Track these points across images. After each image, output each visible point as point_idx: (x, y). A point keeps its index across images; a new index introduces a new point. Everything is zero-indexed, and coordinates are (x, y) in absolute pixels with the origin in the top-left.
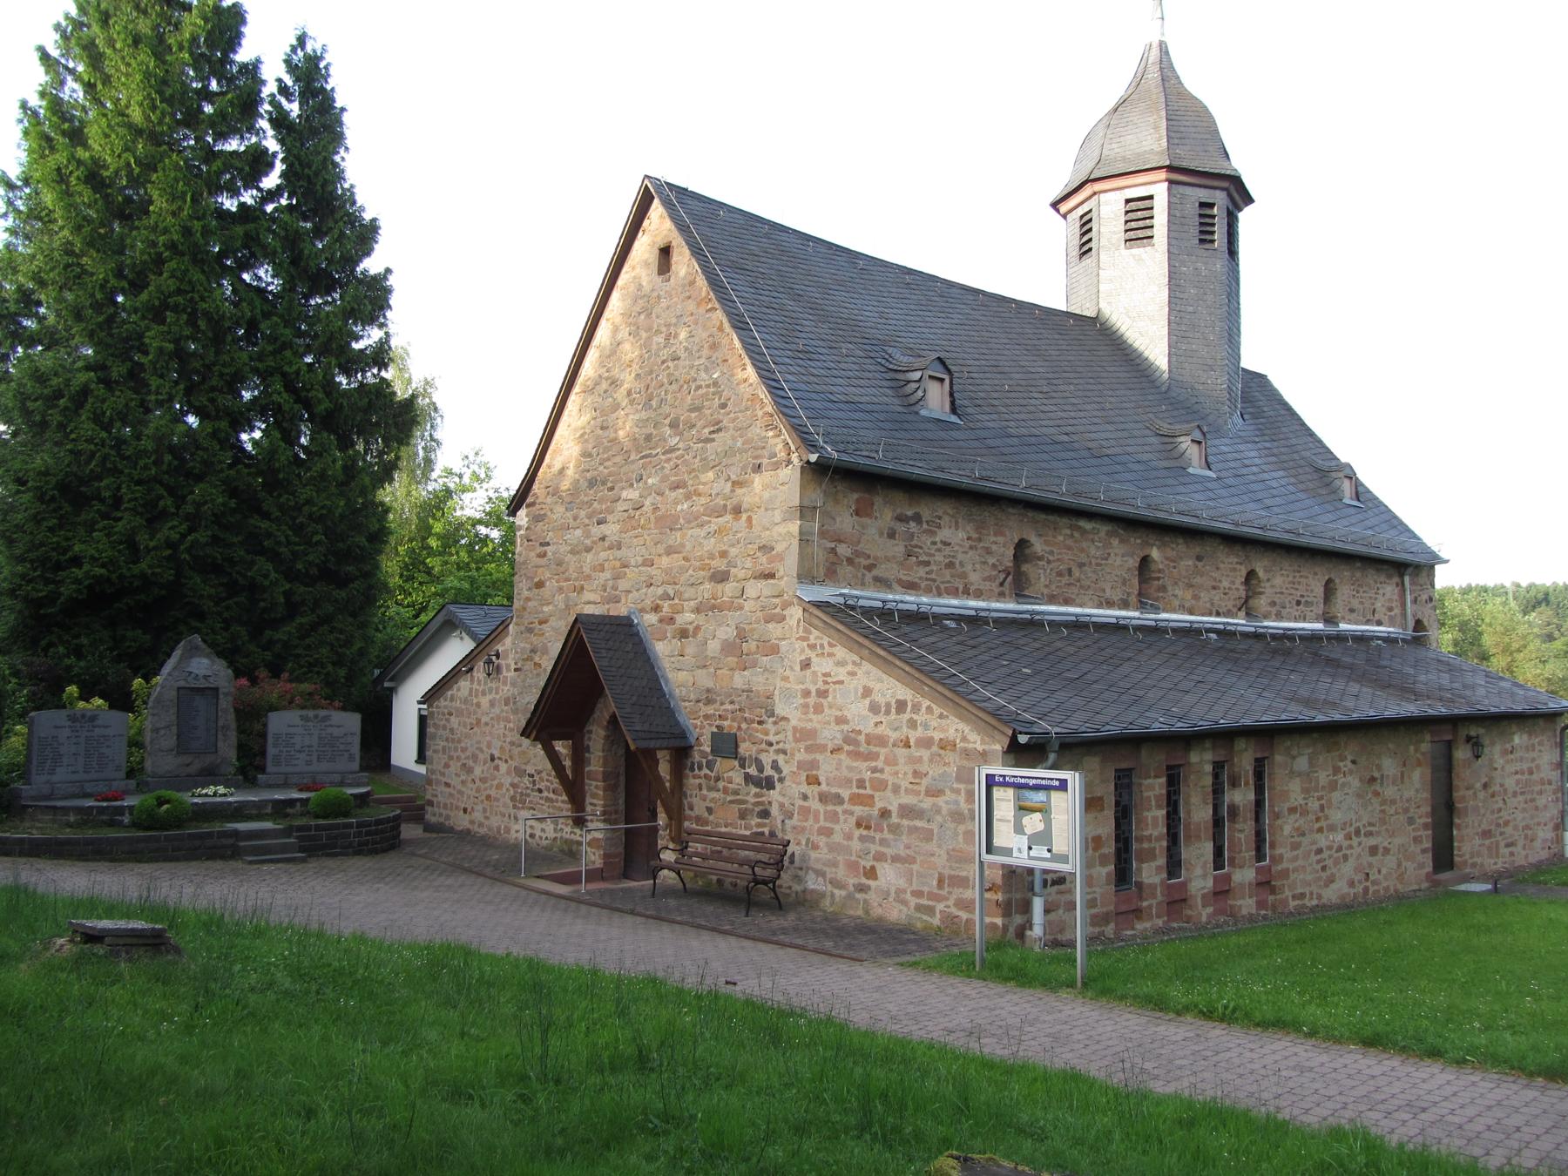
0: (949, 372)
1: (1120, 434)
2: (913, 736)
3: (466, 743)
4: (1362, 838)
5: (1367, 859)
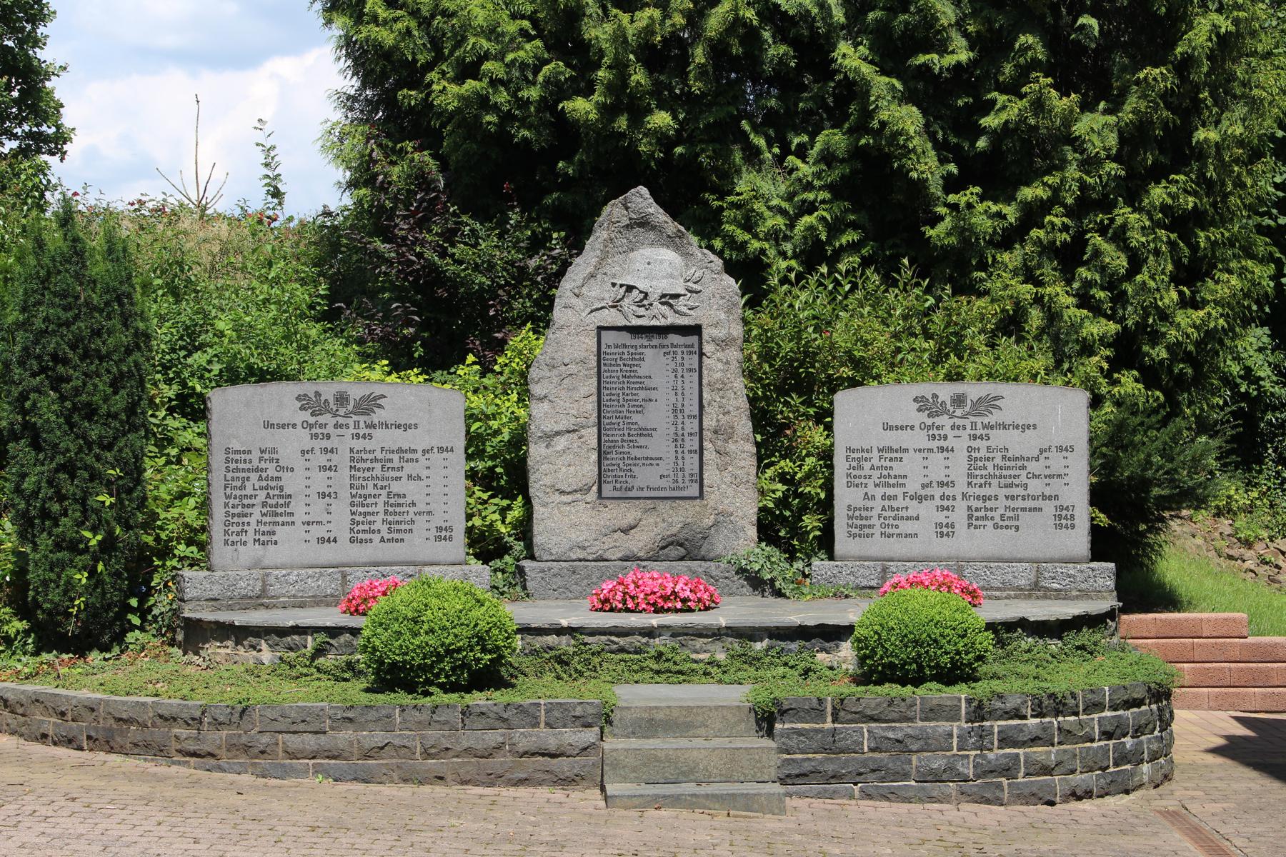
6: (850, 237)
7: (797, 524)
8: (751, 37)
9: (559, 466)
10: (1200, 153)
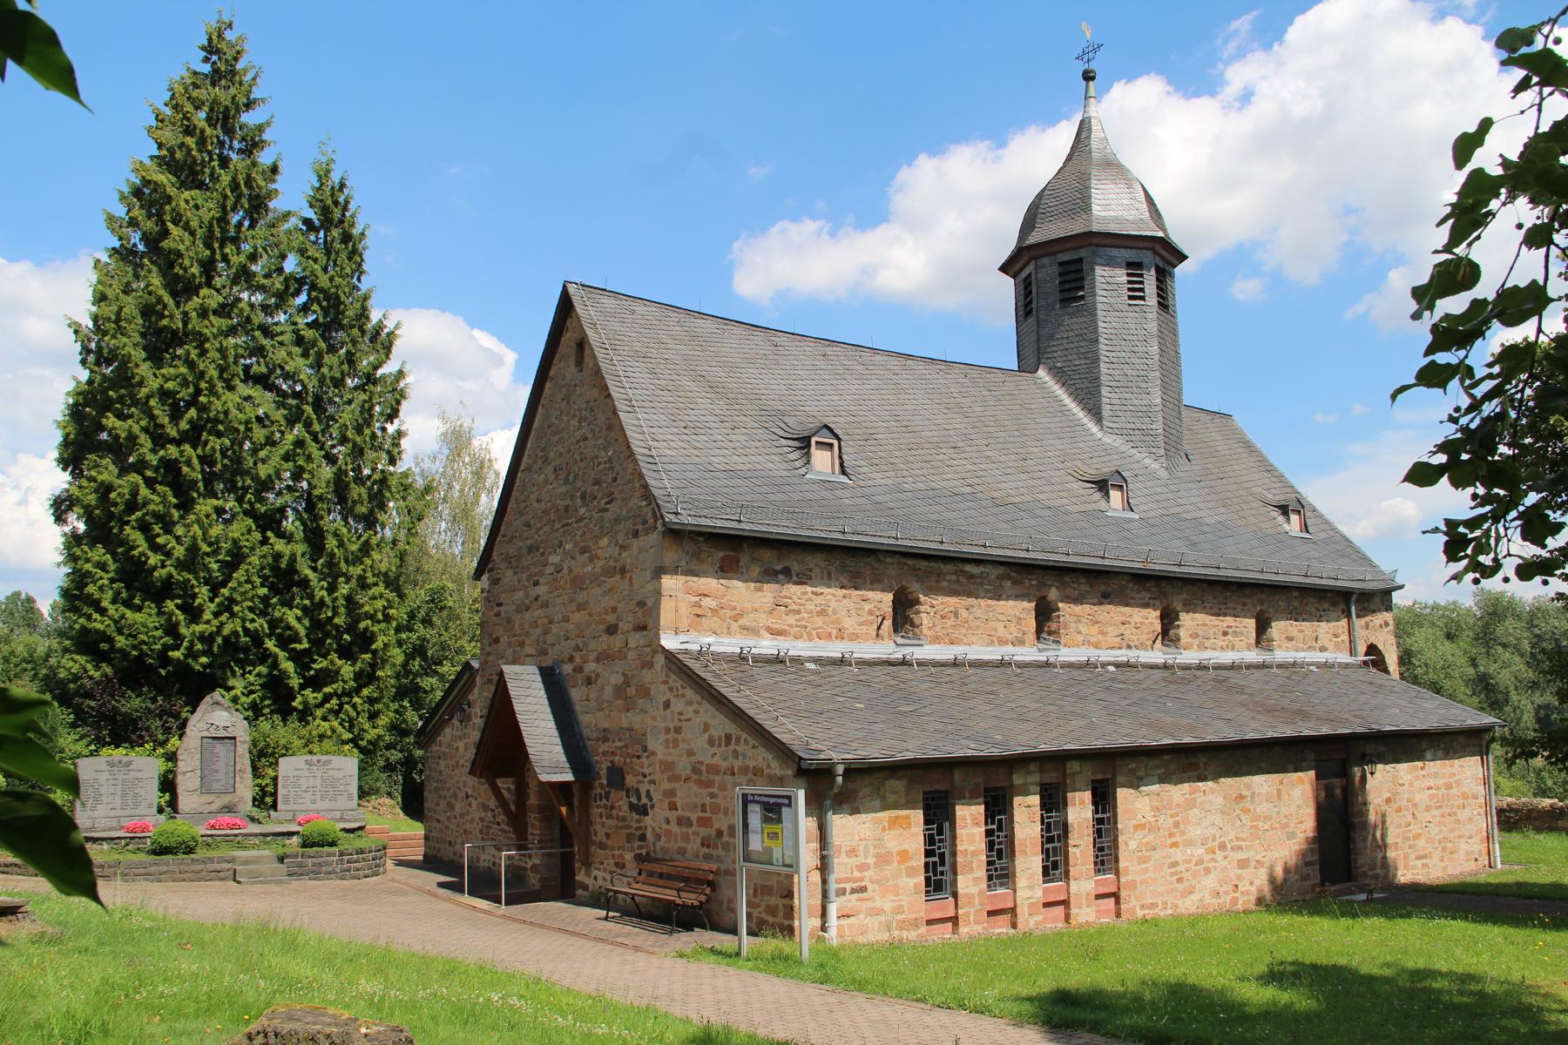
0: (839, 440)
1: (1034, 482)
2: (737, 764)
3: (450, 783)
4: (1229, 852)
5: (1234, 872)
6: (267, 702)
7: (266, 799)
9: (187, 783)
10: (378, 678)
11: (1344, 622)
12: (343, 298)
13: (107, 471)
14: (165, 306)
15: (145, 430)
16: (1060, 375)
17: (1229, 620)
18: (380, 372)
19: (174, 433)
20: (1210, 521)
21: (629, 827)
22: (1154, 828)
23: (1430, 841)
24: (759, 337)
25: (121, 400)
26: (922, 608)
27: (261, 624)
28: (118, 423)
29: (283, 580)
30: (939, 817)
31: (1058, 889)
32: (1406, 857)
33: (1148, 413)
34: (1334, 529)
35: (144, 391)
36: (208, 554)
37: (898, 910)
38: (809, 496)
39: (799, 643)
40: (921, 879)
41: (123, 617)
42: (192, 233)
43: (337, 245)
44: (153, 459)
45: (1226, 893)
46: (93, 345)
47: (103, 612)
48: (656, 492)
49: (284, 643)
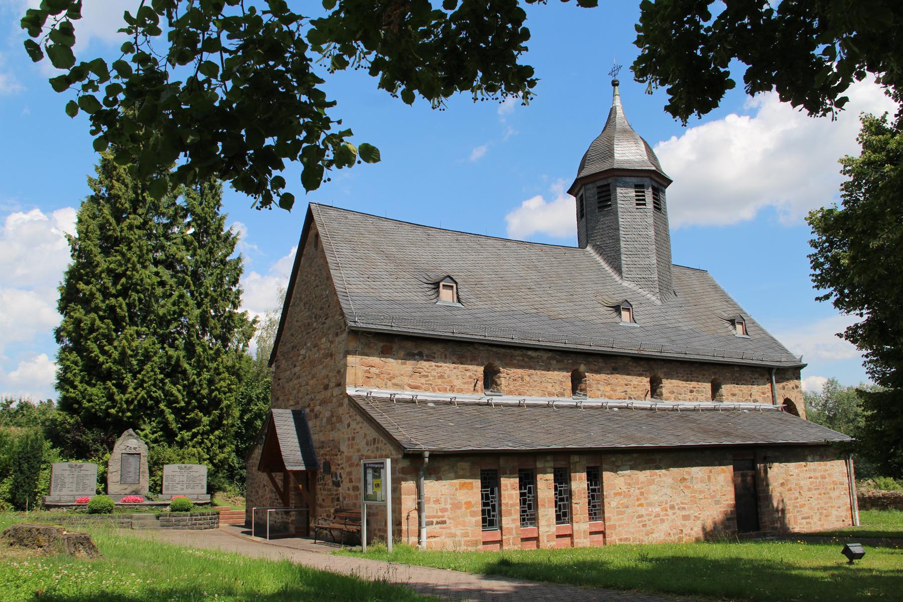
0: (456, 283)
5: (679, 522)
7: (156, 488)
8: (145, 401)
9: (113, 478)
10: (224, 425)
11: (768, 386)
12: (209, 219)
13: (79, 313)
14: (111, 225)
15: (99, 290)
16: (599, 249)
17: (694, 384)
18: (228, 259)
19: (114, 291)
20: (685, 328)
21: (332, 494)
22: (627, 495)
23: (811, 508)
24: (419, 231)
25: (87, 274)
26: (502, 375)
27: (159, 394)
28: (85, 287)
29: (173, 371)
30: (490, 485)
31: (566, 528)
32: (795, 517)
33: (648, 268)
34: (765, 333)
35: (99, 269)
36: (131, 356)
37: (466, 535)
38: (437, 314)
39: (427, 393)
40: (480, 518)
41: (86, 390)
42: (126, 186)
43: (207, 191)
44: (103, 306)
45: (674, 534)
46: (77, 247)
47: (75, 387)
48: (345, 311)
49: (169, 405)
